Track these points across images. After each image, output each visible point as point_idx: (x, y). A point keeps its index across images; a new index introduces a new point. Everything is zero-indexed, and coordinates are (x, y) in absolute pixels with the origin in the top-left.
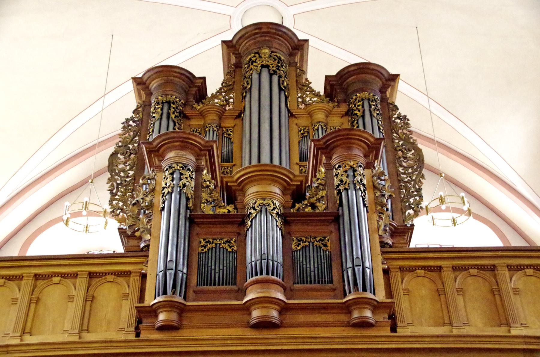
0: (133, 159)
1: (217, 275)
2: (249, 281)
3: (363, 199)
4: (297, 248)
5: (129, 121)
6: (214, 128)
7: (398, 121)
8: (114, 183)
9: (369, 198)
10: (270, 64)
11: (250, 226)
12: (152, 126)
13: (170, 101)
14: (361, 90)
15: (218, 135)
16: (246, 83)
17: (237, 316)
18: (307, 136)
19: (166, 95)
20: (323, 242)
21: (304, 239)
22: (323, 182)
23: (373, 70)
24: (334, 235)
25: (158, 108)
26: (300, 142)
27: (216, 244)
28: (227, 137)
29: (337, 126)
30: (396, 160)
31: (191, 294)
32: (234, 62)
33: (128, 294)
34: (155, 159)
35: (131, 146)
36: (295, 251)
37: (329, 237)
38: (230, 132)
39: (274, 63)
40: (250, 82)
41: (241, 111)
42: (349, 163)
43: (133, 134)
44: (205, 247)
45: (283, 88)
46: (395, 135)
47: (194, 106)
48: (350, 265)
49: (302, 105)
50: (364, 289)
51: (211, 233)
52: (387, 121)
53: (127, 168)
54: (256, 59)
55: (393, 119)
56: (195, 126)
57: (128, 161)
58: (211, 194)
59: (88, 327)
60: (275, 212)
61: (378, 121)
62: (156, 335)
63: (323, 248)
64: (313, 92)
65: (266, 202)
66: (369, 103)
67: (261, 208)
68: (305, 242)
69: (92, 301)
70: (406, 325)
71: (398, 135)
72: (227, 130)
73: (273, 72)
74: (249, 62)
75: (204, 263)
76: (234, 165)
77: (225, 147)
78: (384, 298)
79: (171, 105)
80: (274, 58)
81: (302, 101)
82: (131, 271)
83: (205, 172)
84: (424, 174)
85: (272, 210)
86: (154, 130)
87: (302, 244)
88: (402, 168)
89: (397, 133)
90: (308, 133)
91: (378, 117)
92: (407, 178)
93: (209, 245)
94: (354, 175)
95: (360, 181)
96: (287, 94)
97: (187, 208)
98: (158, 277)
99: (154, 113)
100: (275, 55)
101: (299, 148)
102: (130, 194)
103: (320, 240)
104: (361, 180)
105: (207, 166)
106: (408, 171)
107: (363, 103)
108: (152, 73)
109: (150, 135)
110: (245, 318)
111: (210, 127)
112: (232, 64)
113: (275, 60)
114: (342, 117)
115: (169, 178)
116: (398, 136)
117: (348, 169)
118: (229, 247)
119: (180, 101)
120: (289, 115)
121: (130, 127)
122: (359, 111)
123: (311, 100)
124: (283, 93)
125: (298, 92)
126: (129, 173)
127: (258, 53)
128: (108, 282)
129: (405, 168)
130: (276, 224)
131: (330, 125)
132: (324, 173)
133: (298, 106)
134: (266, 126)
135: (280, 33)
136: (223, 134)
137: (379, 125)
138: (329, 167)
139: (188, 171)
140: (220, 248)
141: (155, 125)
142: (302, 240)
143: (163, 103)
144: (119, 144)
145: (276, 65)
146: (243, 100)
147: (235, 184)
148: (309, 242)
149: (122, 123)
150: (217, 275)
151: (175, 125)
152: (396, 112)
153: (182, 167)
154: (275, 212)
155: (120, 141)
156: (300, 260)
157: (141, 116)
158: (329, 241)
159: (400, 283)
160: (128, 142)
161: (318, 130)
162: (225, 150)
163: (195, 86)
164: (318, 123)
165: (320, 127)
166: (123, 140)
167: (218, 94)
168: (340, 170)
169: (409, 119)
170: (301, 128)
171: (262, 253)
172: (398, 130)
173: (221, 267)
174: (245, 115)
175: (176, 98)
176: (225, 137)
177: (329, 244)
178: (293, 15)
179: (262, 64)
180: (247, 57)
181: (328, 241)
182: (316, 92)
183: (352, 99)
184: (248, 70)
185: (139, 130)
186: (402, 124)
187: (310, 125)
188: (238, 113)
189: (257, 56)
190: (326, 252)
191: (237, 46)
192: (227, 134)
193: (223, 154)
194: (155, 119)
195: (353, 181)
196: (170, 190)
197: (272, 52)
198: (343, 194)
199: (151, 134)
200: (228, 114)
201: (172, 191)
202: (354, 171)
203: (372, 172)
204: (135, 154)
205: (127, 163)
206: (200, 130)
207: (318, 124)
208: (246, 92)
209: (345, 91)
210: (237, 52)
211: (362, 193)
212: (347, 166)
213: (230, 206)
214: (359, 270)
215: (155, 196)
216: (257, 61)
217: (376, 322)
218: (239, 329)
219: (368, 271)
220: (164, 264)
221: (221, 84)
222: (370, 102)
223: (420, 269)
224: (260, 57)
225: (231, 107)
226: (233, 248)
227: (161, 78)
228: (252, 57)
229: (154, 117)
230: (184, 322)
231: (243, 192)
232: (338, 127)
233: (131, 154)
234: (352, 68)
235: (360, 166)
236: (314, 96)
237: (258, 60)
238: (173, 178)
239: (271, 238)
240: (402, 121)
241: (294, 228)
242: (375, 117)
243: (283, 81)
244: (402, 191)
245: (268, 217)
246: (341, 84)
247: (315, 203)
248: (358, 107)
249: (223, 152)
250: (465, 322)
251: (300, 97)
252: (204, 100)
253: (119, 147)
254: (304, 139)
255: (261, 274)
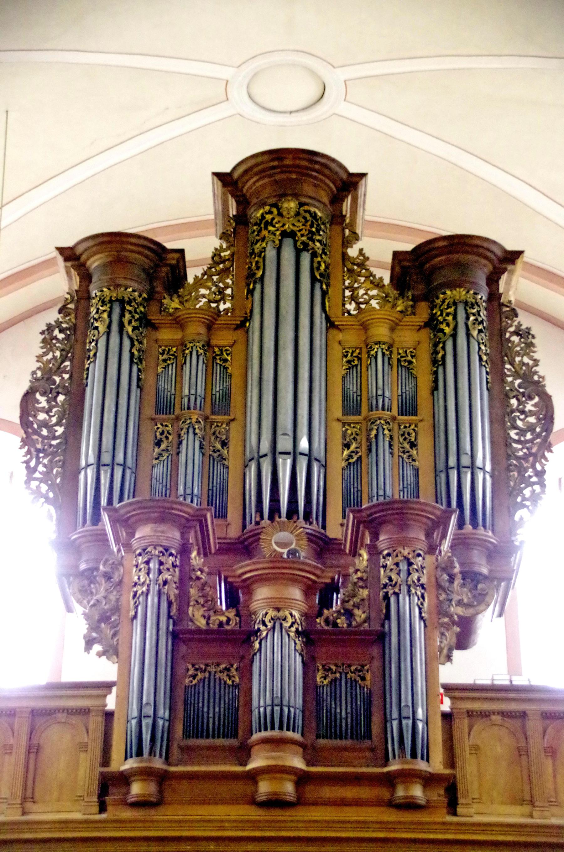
0: (63, 405)
1: (211, 721)
2: (256, 736)
3: (420, 609)
4: (323, 683)
5: (53, 331)
6: (199, 349)
7: (515, 339)
8: (33, 450)
9: (429, 605)
10: (298, 229)
11: (258, 650)
12: (93, 344)
13: (123, 297)
14: (453, 285)
15: (205, 361)
16: (254, 264)
17: (240, 788)
18: (356, 366)
19: (117, 286)
20: (360, 674)
21: (334, 668)
22: (365, 576)
23: (478, 246)
24: (376, 664)
25: (104, 311)
26: (344, 377)
27: (210, 673)
28: (221, 365)
29: (409, 348)
30: (507, 416)
31: (176, 752)
32: (235, 213)
33: (87, 743)
34: (121, 531)
35: (57, 379)
36: (320, 687)
37: (368, 666)
38: (226, 356)
39: (303, 227)
40: (261, 265)
41: (246, 317)
42: (402, 551)
43: (61, 355)
44: (194, 676)
45: (319, 277)
46: (508, 366)
47: (165, 301)
48: (395, 715)
49: (350, 303)
50: (414, 755)
51: (203, 656)
52: (496, 338)
53: (52, 421)
54: (273, 219)
55: (508, 335)
56: (165, 343)
57: (54, 407)
58: (202, 589)
59: (33, 793)
60: (293, 629)
61: (479, 344)
62: (127, 814)
63: (360, 682)
64: (371, 278)
65: (280, 614)
66: (466, 310)
67: (275, 623)
68: (335, 673)
69: (37, 753)
70: (470, 802)
71: (514, 368)
72: (221, 351)
73: (302, 247)
74: (261, 221)
75: (193, 702)
76: (233, 420)
77: (218, 386)
78: (442, 767)
79: (125, 307)
80: (305, 218)
81: (352, 295)
82: (91, 708)
83: (194, 554)
84: (552, 442)
85: (290, 627)
86: (98, 354)
87: (330, 675)
88: (516, 431)
89: (512, 364)
90: (360, 359)
91: (480, 338)
92: (522, 451)
93: (199, 674)
94: (408, 570)
95: (416, 581)
96: (324, 287)
97: (169, 617)
98: (129, 724)
99: (96, 320)
100: (306, 211)
101: (343, 389)
102: (60, 469)
103: (356, 669)
104: (419, 580)
105: (197, 545)
106: (525, 436)
107: (456, 310)
108: (90, 243)
109: (91, 362)
110: (249, 789)
111: (192, 348)
112: (231, 216)
113: (307, 221)
114: (418, 330)
115: (143, 569)
116: (513, 370)
117: (401, 560)
118: (228, 677)
119: (140, 296)
120: (328, 325)
121: (54, 341)
122: (448, 325)
123: (366, 294)
124: (318, 285)
125: (345, 278)
126: (56, 431)
127: (275, 205)
128: (58, 722)
129: (522, 432)
130: (295, 647)
131: (396, 345)
132: (367, 561)
133: (344, 305)
134: (287, 356)
135: (317, 167)
136: (214, 358)
137: (480, 353)
138: (374, 551)
139: (171, 557)
140: (215, 679)
141: (99, 345)
142: (330, 669)
143: (111, 301)
144: (36, 374)
145: (307, 232)
146: (249, 296)
147: (238, 580)
148: (341, 673)
149: (41, 333)
150: (211, 721)
151: (132, 345)
152: (514, 322)
153: (161, 552)
154: (293, 629)
155: (39, 368)
156: (327, 701)
157: (73, 320)
158: (369, 672)
159: (466, 735)
160: (53, 371)
161: (376, 358)
162: (218, 389)
163: (167, 265)
164: (376, 344)
165: (380, 350)
166: (44, 366)
167: (206, 277)
168: (388, 560)
169: (535, 336)
170: (347, 350)
171: (275, 696)
172: (514, 358)
173: (217, 710)
174: (251, 324)
175: (134, 291)
176: (217, 364)
177: (368, 677)
178: (345, 81)
179: (282, 229)
180: (258, 210)
181: (368, 671)
182: (377, 277)
183: (438, 298)
184: (258, 238)
185: (71, 348)
186: (523, 345)
187: (363, 345)
188: (240, 321)
189: (275, 210)
190: (364, 690)
191: (240, 184)
192: (220, 359)
193: (214, 397)
194: (99, 333)
195: (407, 581)
196: (144, 589)
197: (301, 205)
198: (393, 600)
199: (92, 360)
200: (223, 322)
201: (148, 590)
202: (410, 564)
203: (437, 560)
204: (65, 395)
205: (52, 412)
206: (174, 349)
207: (377, 346)
208: (255, 283)
209: (428, 278)
210: (239, 193)
211: (419, 599)
212: (399, 555)
213: (230, 610)
214: (407, 723)
215: (123, 592)
216: (274, 222)
217: (428, 801)
218: (241, 807)
219: (420, 725)
220: (137, 708)
221: (210, 259)
222: (468, 309)
223: (496, 714)
224: (280, 214)
225: (228, 305)
226: (233, 679)
227: (107, 254)
228: (267, 213)
229: (96, 328)
230: (168, 795)
231: (249, 592)
232: (411, 350)
233: (58, 393)
234: (441, 244)
235: (419, 555)
236: (372, 286)
237: (276, 220)
238: (149, 569)
239: (287, 672)
240: (522, 340)
241: (322, 651)
242: (473, 337)
243: (319, 263)
244: (512, 474)
245: (283, 637)
246: (422, 265)
247: (352, 610)
248: (447, 318)
249: (214, 393)
250: (552, 800)
251: (347, 288)
252: (182, 290)
253: (37, 380)
254: (351, 372)
255: (273, 728)
